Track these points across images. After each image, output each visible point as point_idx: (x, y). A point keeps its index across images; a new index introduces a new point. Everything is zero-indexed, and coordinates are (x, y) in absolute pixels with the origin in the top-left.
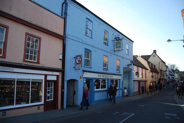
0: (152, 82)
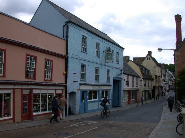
0: (145, 91)
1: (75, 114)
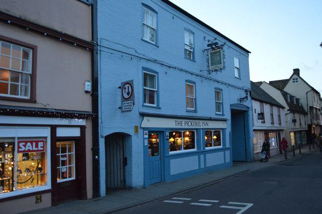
1: (130, 188)
